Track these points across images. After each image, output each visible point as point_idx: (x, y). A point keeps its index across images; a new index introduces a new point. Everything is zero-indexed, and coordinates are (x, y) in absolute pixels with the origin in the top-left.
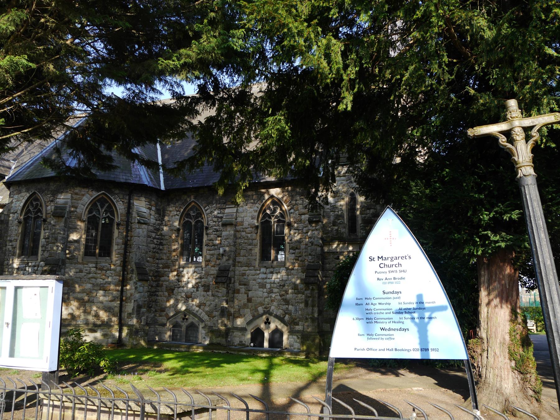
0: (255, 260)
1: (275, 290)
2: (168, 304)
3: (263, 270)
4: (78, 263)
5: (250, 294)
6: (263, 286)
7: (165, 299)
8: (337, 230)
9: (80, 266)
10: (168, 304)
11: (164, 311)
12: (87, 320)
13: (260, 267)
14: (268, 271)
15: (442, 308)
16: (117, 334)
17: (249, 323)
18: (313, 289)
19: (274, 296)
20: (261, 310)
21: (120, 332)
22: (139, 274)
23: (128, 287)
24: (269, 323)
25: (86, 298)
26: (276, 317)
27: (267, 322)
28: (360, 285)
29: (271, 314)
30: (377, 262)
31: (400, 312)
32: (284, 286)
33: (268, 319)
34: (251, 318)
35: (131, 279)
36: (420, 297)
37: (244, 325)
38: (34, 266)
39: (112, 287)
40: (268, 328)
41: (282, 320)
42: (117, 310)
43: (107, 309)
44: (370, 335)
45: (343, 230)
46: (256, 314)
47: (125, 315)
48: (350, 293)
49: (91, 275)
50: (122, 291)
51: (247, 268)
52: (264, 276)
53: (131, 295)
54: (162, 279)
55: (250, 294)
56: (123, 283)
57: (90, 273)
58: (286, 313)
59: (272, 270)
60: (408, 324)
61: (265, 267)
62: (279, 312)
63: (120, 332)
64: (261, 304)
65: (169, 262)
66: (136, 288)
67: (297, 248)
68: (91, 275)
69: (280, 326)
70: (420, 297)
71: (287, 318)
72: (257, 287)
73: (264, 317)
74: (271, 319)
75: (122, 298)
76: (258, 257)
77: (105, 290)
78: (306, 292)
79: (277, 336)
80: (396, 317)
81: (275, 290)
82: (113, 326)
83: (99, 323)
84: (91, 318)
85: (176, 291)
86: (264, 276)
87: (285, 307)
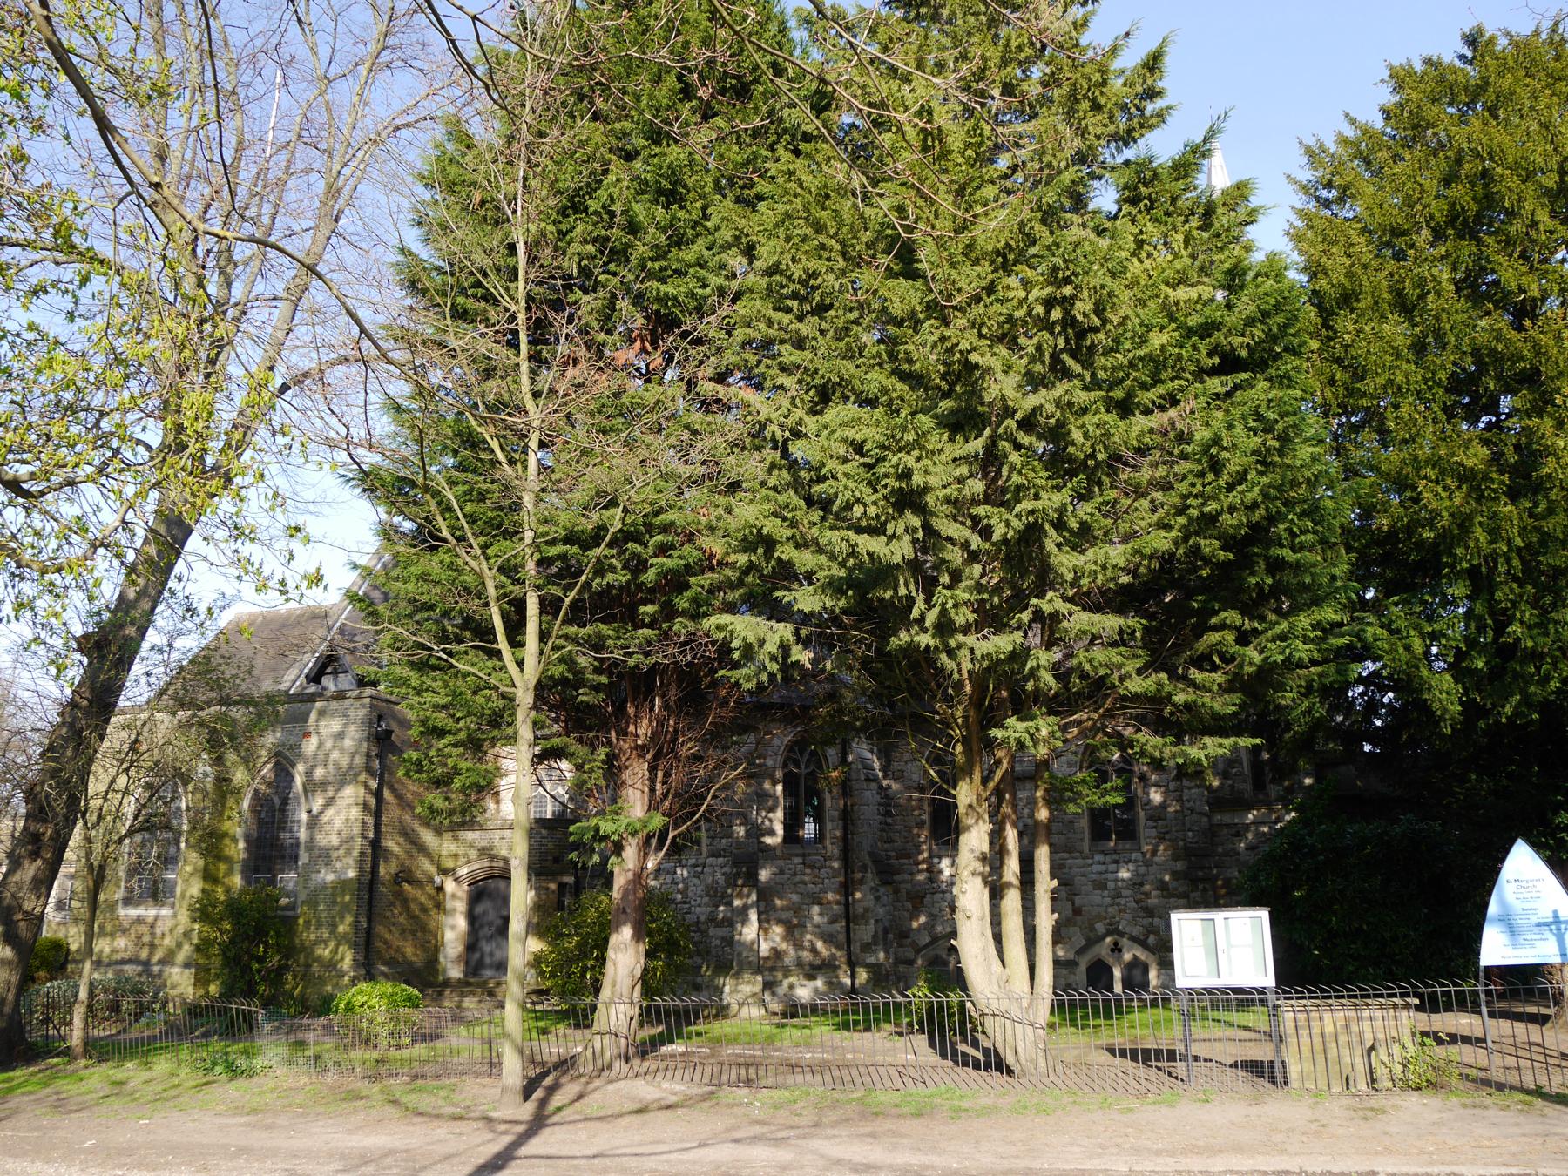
0: (1082, 840)
1: (1126, 893)
2: (915, 924)
3: (1099, 857)
4: (776, 857)
5: (1077, 900)
6: (1101, 886)
7: (907, 915)
8: (1232, 786)
9: (780, 862)
10: (915, 924)
11: (907, 937)
12: (799, 958)
13: (1092, 853)
14: (1108, 858)
15: (1507, 921)
16: (848, 981)
17: (1081, 952)
18: (1205, 890)
19: (1123, 901)
20: (1100, 927)
21: (853, 976)
22: (880, 873)
23: (858, 895)
24: (1120, 950)
25: (795, 921)
26: (1133, 939)
27: (1116, 949)
28: (1502, 903)
29: (1121, 934)
30: (1514, 885)
31: (1539, 925)
32: (1141, 884)
33: (1116, 944)
34: (1084, 942)
35: (862, 881)
36: (1555, 912)
37: (1071, 956)
38: (695, 866)
39: (830, 896)
40: (1119, 960)
41: (1143, 944)
42: (842, 938)
43: (829, 939)
44: (1514, 946)
45: (1241, 786)
46: (1092, 935)
47: (855, 948)
48: (1493, 908)
49: (798, 878)
50: (847, 905)
51: (1066, 855)
52: (1103, 868)
53: (867, 910)
54: (897, 878)
55: (1077, 900)
56: (847, 889)
57: (795, 874)
58: (1149, 932)
59: (1115, 857)
60: (1548, 935)
61: (1102, 852)
62: (1137, 931)
63: (853, 976)
64: (1100, 918)
65: (909, 846)
66: (877, 898)
67: (1160, 819)
68: (798, 878)
69: (1142, 955)
70: (1555, 912)
71: (1152, 939)
72: (1090, 888)
73: (1108, 940)
74: (1125, 941)
75: (849, 916)
76: (1087, 835)
77: (820, 904)
78: (1193, 895)
79: (1137, 973)
80: (1536, 929)
81: (1126, 893)
82: (838, 967)
83: (818, 962)
84: (806, 955)
85: (928, 898)
86: (1103, 868)
87: (1146, 921)
